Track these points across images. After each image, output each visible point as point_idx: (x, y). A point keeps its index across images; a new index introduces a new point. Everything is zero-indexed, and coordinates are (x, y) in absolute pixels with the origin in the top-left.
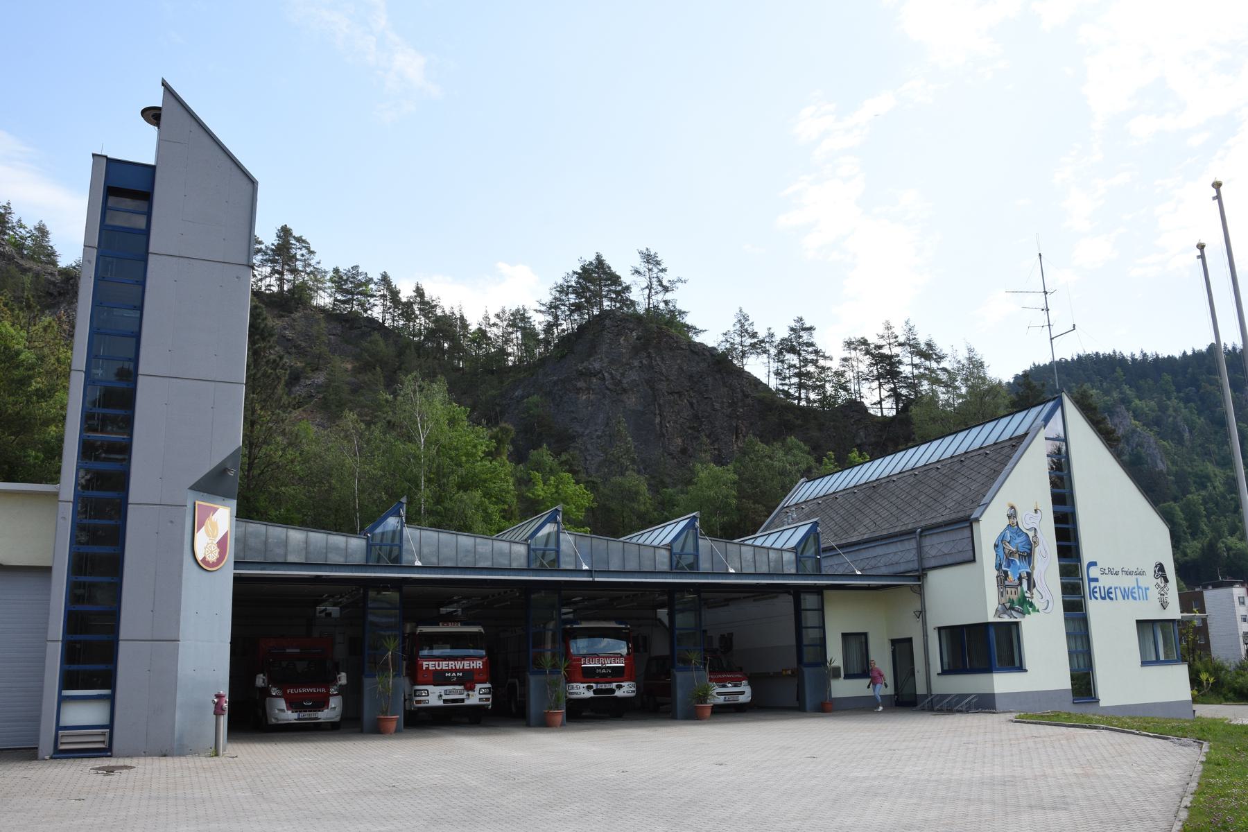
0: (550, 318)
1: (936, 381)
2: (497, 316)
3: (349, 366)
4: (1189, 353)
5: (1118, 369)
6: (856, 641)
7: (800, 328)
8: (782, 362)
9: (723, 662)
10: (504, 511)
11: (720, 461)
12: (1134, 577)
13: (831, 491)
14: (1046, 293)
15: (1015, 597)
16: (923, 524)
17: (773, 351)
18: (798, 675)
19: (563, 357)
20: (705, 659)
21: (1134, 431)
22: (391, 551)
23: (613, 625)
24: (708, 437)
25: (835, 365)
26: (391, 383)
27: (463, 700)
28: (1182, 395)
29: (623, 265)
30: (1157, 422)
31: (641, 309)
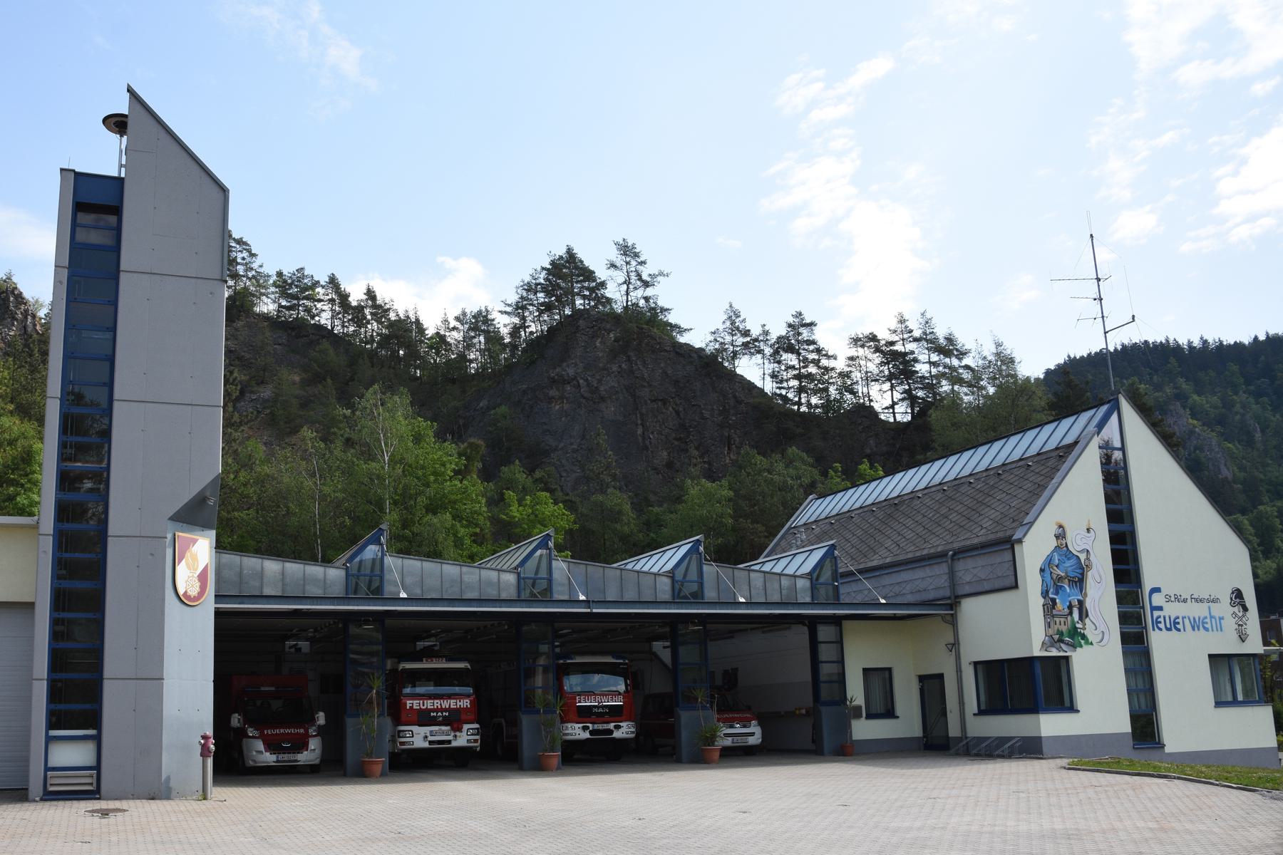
0: (516, 320)
1: (956, 380)
2: (457, 319)
3: (297, 378)
4: (1262, 337)
5: (1172, 360)
6: (879, 679)
7: (799, 324)
8: (779, 362)
9: (731, 697)
10: (475, 534)
11: (711, 477)
12: (1206, 605)
13: (845, 509)
14: (1098, 280)
15: (1064, 628)
16: (956, 545)
17: (768, 351)
18: (814, 713)
19: (533, 363)
20: (712, 696)
21: (1192, 432)
22: (370, 582)
23: (610, 660)
24: (697, 448)
25: (840, 365)
26: (346, 398)
27: (449, 742)
28: (1252, 388)
29: (596, 258)
30: (1221, 421)
31: (618, 308)
